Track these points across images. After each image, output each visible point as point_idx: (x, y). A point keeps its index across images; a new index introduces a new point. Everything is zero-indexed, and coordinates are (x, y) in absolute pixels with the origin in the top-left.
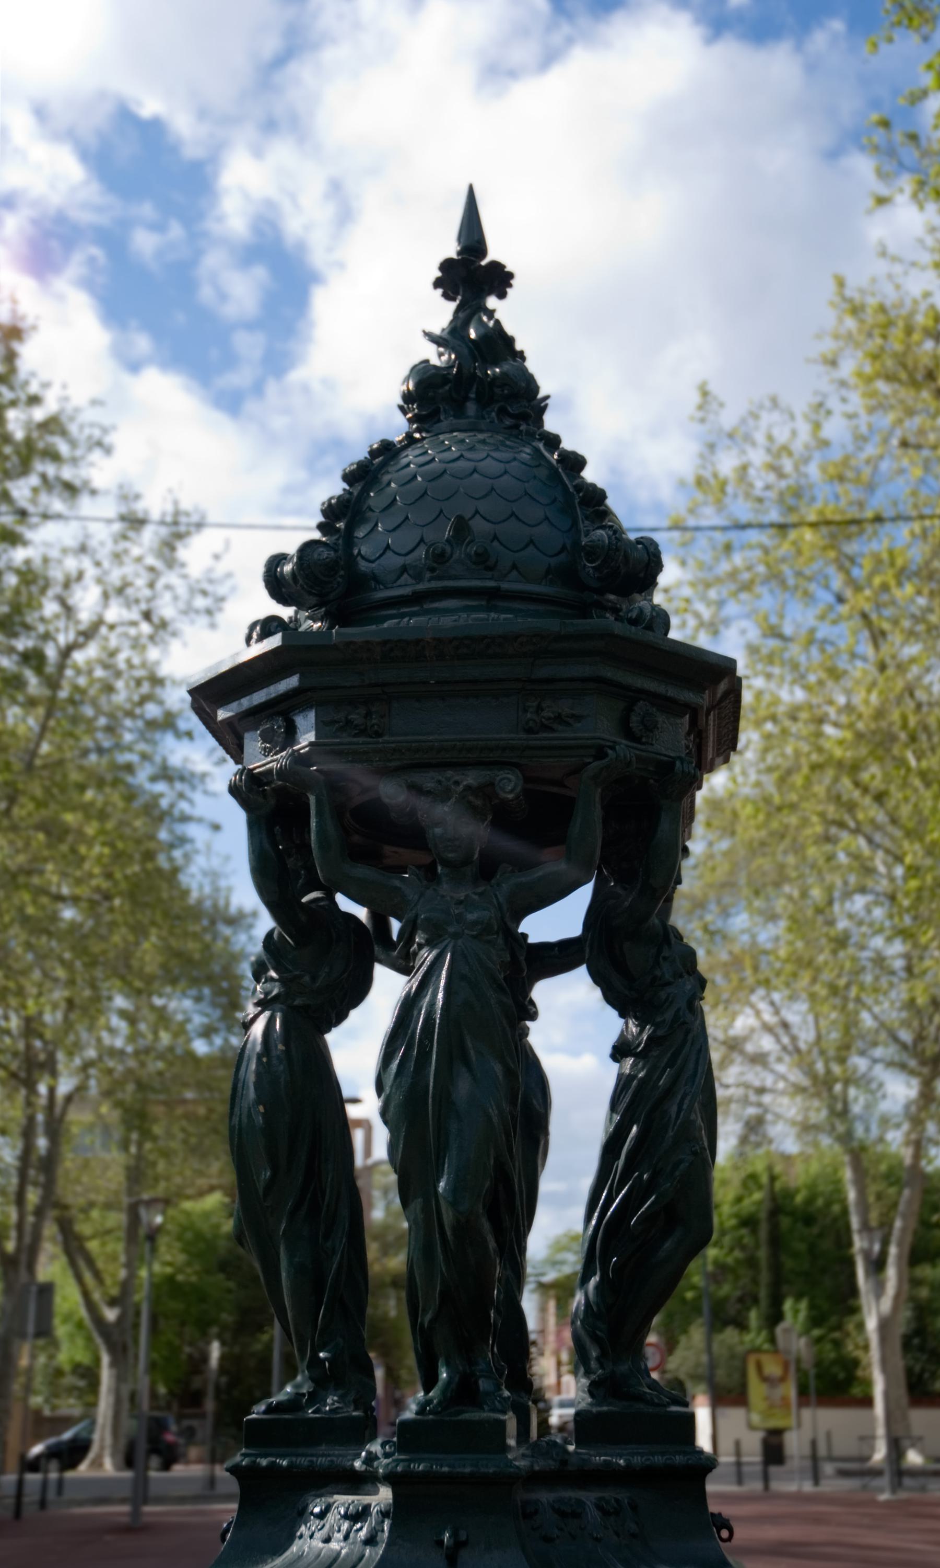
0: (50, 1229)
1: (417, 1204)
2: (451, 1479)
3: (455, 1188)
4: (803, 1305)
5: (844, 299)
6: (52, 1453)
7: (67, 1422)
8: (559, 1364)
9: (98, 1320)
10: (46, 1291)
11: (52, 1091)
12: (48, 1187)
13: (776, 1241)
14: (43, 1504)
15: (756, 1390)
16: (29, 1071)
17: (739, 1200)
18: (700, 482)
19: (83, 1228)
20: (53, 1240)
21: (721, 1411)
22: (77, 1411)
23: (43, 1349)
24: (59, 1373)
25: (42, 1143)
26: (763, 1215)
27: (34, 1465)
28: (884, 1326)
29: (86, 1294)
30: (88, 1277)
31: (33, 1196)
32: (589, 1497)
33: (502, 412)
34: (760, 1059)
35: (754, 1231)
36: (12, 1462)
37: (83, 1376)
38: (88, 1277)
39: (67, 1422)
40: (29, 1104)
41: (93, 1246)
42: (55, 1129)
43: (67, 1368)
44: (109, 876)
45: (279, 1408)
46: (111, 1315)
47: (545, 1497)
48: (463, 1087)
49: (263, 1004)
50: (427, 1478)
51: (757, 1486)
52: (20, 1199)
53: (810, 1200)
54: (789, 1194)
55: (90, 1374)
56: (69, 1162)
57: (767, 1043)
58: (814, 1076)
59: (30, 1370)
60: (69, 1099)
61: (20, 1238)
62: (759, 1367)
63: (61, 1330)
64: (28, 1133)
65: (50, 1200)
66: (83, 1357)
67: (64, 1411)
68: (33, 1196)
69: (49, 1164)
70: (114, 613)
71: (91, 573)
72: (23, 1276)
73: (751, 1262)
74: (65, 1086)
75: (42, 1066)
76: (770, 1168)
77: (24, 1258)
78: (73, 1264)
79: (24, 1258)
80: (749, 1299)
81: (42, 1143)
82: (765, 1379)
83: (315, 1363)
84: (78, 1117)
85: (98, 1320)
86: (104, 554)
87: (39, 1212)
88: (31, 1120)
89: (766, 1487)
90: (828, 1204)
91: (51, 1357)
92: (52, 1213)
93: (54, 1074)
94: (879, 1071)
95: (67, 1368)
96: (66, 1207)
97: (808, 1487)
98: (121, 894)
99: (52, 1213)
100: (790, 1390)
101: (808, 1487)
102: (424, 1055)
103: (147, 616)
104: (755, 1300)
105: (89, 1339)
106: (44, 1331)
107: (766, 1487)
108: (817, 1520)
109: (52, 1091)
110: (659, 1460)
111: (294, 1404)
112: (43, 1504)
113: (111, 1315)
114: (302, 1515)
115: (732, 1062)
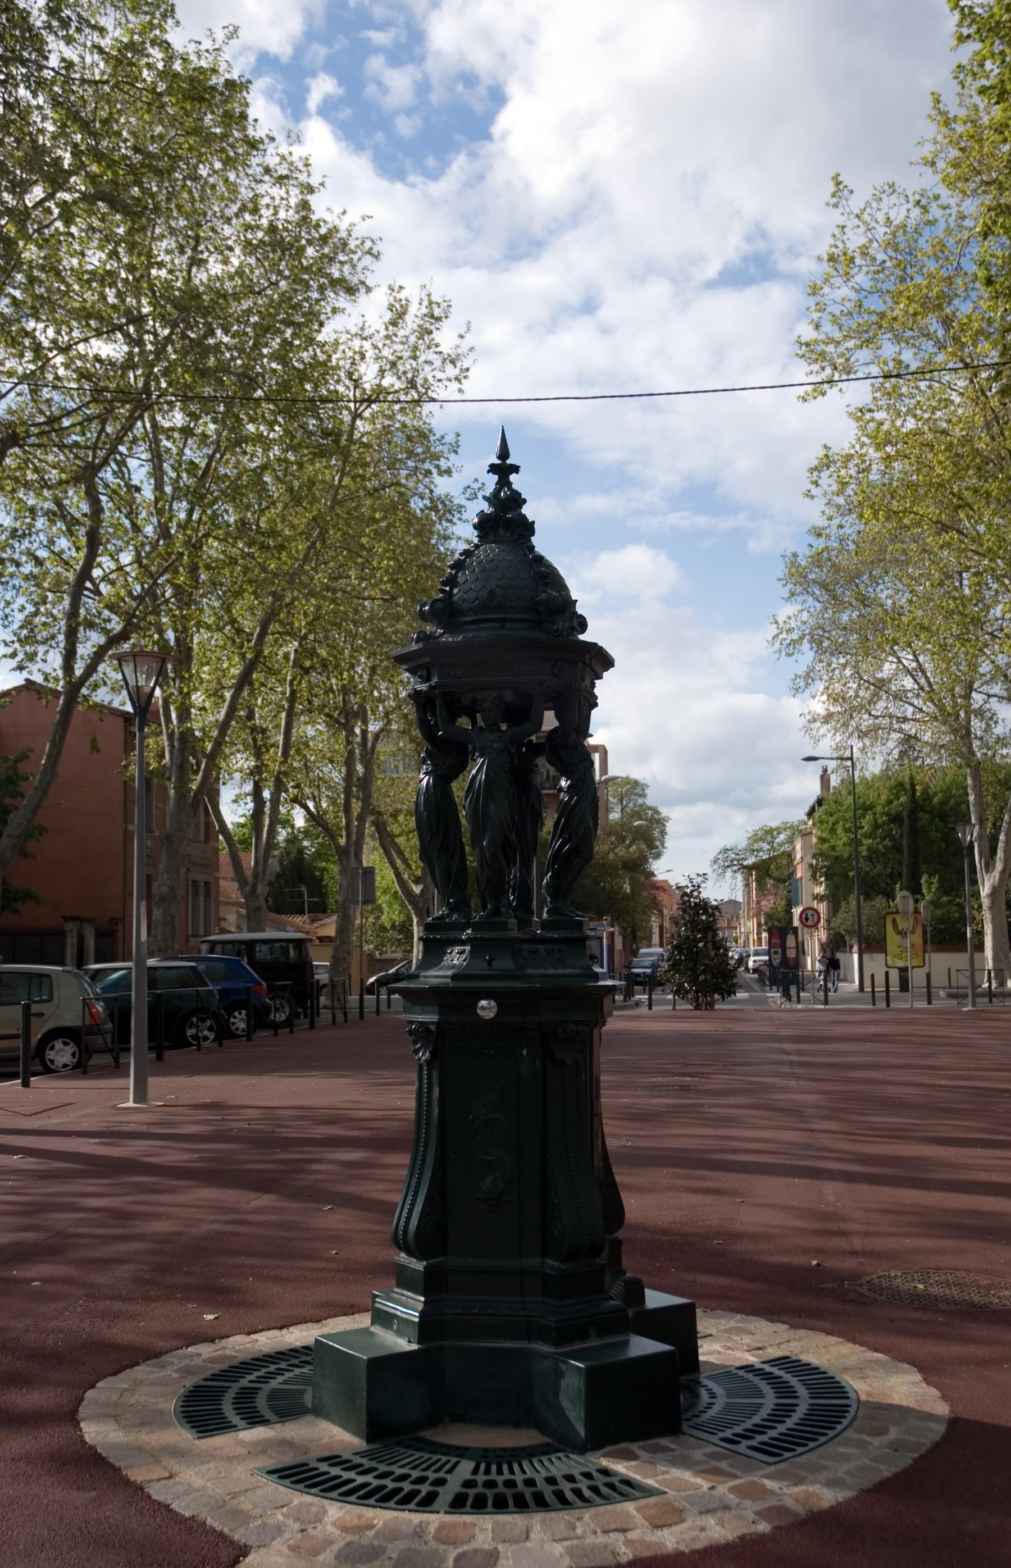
0: (369, 829)
1: (477, 850)
2: (490, 940)
3: (488, 844)
4: (935, 880)
5: (941, 113)
6: (380, 982)
7: (392, 962)
8: (759, 925)
9: (409, 893)
10: (369, 872)
11: (364, 733)
12: (366, 800)
13: (914, 833)
14: (378, 1012)
15: (893, 939)
16: (346, 718)
17: (890, 802)
18: (832, 259)
19: (394, 828)
20: (372, 836)
21: (865, 957)
22: (399, 955)
23: (371, 912)
24: (383, 928)
25: (360, 768)
26: (905, 814)
27: (370, 990)
28: (993, 894)
29: (398, 875)
30: (398, 862)
31: (356, 807)
32: (542, 948)
33: (513, 533)
34: (899, 696)
35: (900, 826)
36: (356, 988)
37: (400, 932)
38: (398, 862)
39: (392, 962)
40: (349, 743)
41: (401, 841)
42: (369, 757)
43: (388, 925)
44: (394, 581)
45: (437, 918)
46: (417, 889)
47: (526, 947)
48: (492, 808)
49: (426, 774)
50: (481, 939)
51: (884, 1005)
52: (347, 809)
53: (943, 803)
54: (927, 796)
55: (405, 929)
56: (379, 783)
57: (908, 683)
58: (941, 708)
59: (361, 927)
60: (377, 736)
61: (349, 836)
62: (894, 921)
63: (382, 900)
64: (349, 763)
65: (368, 808)
66: (398, 918)
67: (389, 956)
68: (356, 807)
69: (366, 783)
70: (388, 381)
71: (370, 354)
72: (353, 863)
73: (898, 849)
74: (373, 727)
75: (356, 715)
76: (912, 778)
77: (352, 850)
78: (387, 853)
79: (352, 850)
80: (894, 876)
81: (360, 768)
82: (901, 933)
83: (449, 903)
84: (384, 749)
85: (409, 893)
86: (379, 340)
87: (361, 818)
88: (351, 753)
89: (888, 1005)
90: (958, 805)
91: (378, 918)
92: (370, 818)
93: (365, 722)
94: (994, 704)
95: (388, 925)
96: (380, 814)
97: (922, 1004)
98: (403, 594)
99: (370, 818)
100: (917, 939)
101: (922, 1004)
102: (478, 797)
103: (412, 384)
104: (900, 875)
105: (403, 906)
106: (370, 898)
107: (888, 1005)
108: (909, 1022)
109: (364, 733)
110: (569, 935)
111: (442, 917)
112: (378, 1012)
113: (417, 889)
114: (445, 953)
115: (880, 699)
